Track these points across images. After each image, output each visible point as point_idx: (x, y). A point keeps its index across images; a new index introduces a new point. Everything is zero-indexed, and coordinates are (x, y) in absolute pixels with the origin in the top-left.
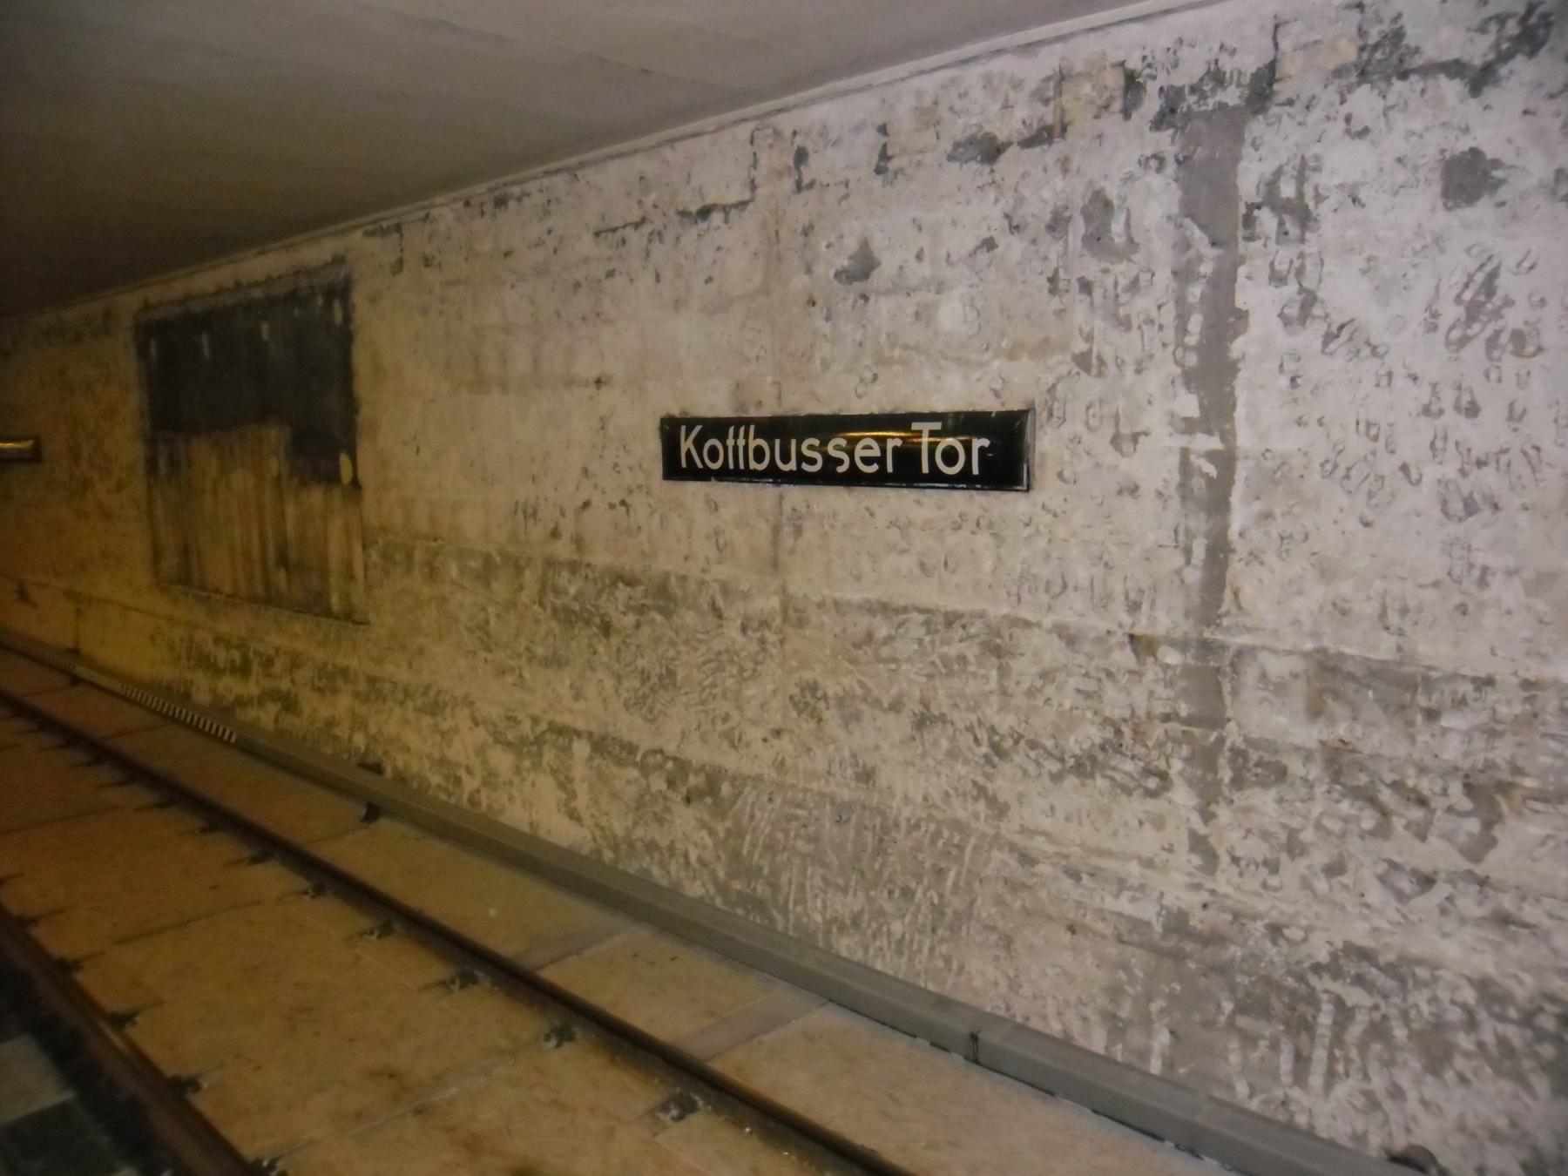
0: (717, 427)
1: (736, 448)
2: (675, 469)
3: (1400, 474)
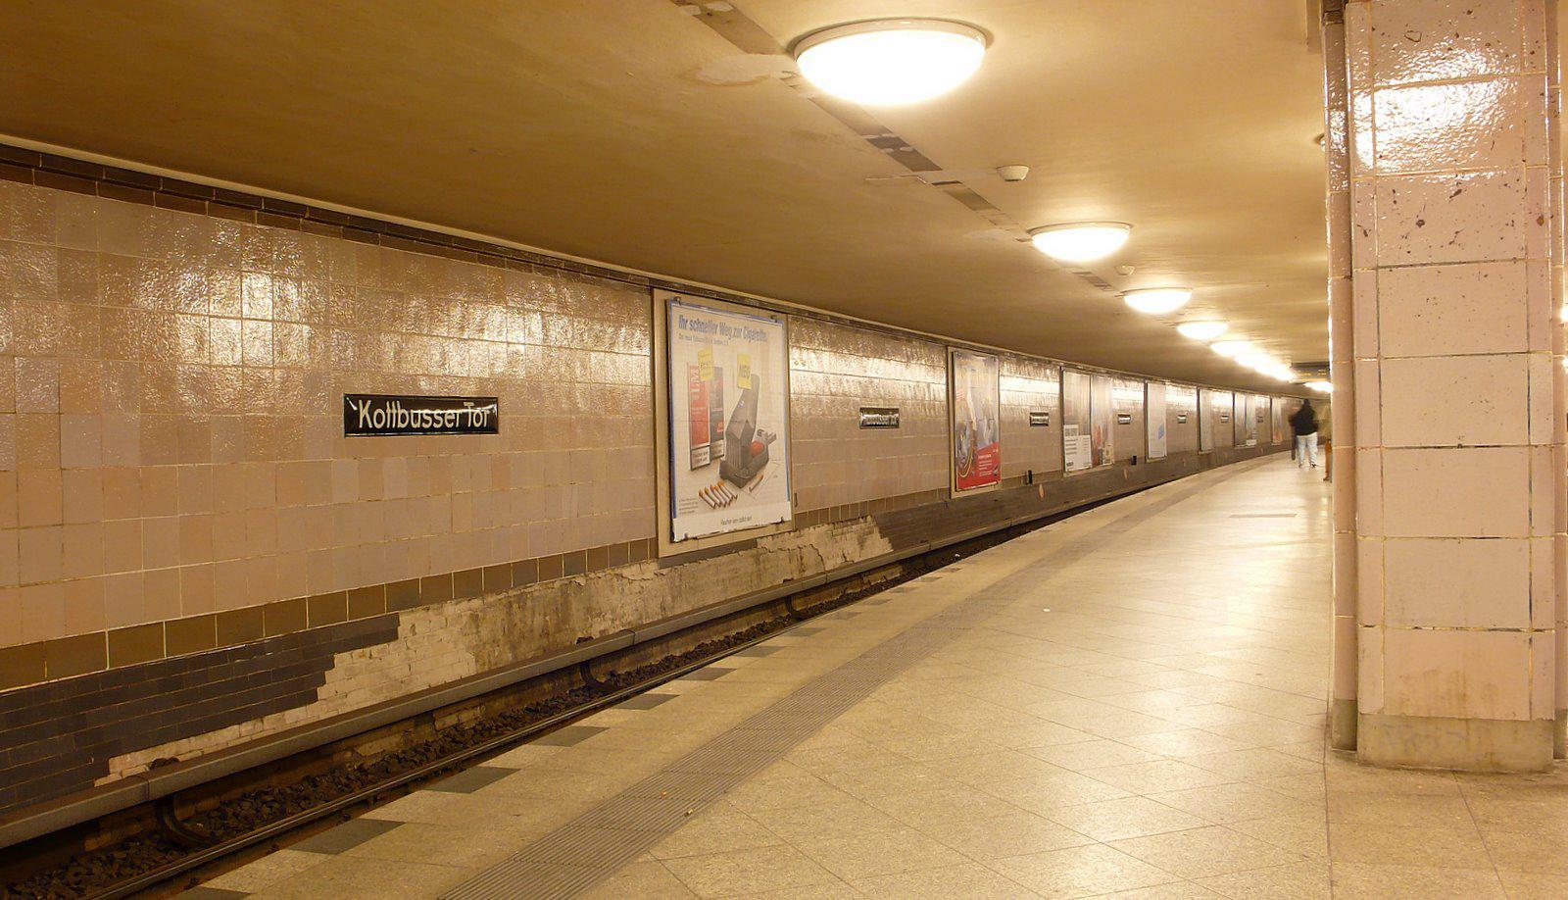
0: (379, 401)
1: (392, 414)
2: (1420, 226)
3: (395, 457)
